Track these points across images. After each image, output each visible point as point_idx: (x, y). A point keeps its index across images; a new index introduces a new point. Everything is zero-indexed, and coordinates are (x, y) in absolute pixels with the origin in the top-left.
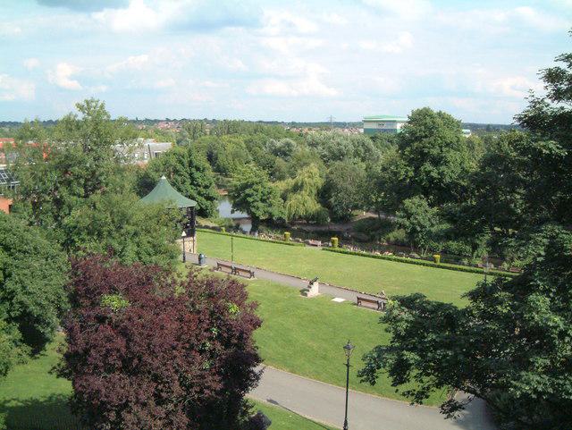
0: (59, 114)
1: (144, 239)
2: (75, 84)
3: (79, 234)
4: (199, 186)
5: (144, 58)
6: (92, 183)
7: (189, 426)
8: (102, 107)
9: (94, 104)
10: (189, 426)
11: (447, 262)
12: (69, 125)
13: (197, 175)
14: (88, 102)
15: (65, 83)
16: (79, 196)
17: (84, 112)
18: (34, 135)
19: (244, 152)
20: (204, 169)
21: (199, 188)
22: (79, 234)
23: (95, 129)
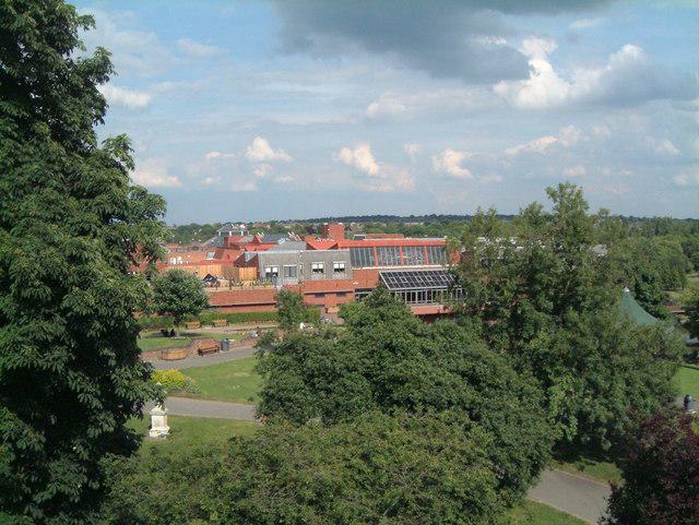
0: (512, 206)
1: (637, 375)
2: (465, 172)
3: (552, 365)
4: (647, 301)
5: (548, 140)
6: (566, 299)
7: (4, 369)
8: (578, 194)
9: (569, 190)
10: (4, 369)
11: (239, 314)
12: (533, 218)
13: (645, 286)
14: (561, 187)
15: (456, 171)
16: (546, 311)
17: (555, 201)
18: (488, 232)
19: (683, 258)
20: (653, 278)
21: (646, 304)
22: (552, 365)
23: (568, 223)
